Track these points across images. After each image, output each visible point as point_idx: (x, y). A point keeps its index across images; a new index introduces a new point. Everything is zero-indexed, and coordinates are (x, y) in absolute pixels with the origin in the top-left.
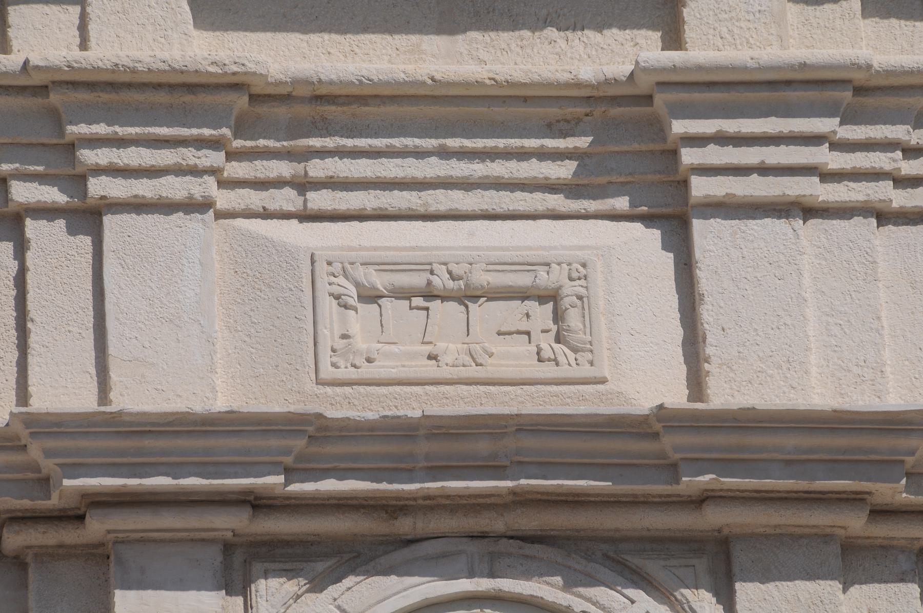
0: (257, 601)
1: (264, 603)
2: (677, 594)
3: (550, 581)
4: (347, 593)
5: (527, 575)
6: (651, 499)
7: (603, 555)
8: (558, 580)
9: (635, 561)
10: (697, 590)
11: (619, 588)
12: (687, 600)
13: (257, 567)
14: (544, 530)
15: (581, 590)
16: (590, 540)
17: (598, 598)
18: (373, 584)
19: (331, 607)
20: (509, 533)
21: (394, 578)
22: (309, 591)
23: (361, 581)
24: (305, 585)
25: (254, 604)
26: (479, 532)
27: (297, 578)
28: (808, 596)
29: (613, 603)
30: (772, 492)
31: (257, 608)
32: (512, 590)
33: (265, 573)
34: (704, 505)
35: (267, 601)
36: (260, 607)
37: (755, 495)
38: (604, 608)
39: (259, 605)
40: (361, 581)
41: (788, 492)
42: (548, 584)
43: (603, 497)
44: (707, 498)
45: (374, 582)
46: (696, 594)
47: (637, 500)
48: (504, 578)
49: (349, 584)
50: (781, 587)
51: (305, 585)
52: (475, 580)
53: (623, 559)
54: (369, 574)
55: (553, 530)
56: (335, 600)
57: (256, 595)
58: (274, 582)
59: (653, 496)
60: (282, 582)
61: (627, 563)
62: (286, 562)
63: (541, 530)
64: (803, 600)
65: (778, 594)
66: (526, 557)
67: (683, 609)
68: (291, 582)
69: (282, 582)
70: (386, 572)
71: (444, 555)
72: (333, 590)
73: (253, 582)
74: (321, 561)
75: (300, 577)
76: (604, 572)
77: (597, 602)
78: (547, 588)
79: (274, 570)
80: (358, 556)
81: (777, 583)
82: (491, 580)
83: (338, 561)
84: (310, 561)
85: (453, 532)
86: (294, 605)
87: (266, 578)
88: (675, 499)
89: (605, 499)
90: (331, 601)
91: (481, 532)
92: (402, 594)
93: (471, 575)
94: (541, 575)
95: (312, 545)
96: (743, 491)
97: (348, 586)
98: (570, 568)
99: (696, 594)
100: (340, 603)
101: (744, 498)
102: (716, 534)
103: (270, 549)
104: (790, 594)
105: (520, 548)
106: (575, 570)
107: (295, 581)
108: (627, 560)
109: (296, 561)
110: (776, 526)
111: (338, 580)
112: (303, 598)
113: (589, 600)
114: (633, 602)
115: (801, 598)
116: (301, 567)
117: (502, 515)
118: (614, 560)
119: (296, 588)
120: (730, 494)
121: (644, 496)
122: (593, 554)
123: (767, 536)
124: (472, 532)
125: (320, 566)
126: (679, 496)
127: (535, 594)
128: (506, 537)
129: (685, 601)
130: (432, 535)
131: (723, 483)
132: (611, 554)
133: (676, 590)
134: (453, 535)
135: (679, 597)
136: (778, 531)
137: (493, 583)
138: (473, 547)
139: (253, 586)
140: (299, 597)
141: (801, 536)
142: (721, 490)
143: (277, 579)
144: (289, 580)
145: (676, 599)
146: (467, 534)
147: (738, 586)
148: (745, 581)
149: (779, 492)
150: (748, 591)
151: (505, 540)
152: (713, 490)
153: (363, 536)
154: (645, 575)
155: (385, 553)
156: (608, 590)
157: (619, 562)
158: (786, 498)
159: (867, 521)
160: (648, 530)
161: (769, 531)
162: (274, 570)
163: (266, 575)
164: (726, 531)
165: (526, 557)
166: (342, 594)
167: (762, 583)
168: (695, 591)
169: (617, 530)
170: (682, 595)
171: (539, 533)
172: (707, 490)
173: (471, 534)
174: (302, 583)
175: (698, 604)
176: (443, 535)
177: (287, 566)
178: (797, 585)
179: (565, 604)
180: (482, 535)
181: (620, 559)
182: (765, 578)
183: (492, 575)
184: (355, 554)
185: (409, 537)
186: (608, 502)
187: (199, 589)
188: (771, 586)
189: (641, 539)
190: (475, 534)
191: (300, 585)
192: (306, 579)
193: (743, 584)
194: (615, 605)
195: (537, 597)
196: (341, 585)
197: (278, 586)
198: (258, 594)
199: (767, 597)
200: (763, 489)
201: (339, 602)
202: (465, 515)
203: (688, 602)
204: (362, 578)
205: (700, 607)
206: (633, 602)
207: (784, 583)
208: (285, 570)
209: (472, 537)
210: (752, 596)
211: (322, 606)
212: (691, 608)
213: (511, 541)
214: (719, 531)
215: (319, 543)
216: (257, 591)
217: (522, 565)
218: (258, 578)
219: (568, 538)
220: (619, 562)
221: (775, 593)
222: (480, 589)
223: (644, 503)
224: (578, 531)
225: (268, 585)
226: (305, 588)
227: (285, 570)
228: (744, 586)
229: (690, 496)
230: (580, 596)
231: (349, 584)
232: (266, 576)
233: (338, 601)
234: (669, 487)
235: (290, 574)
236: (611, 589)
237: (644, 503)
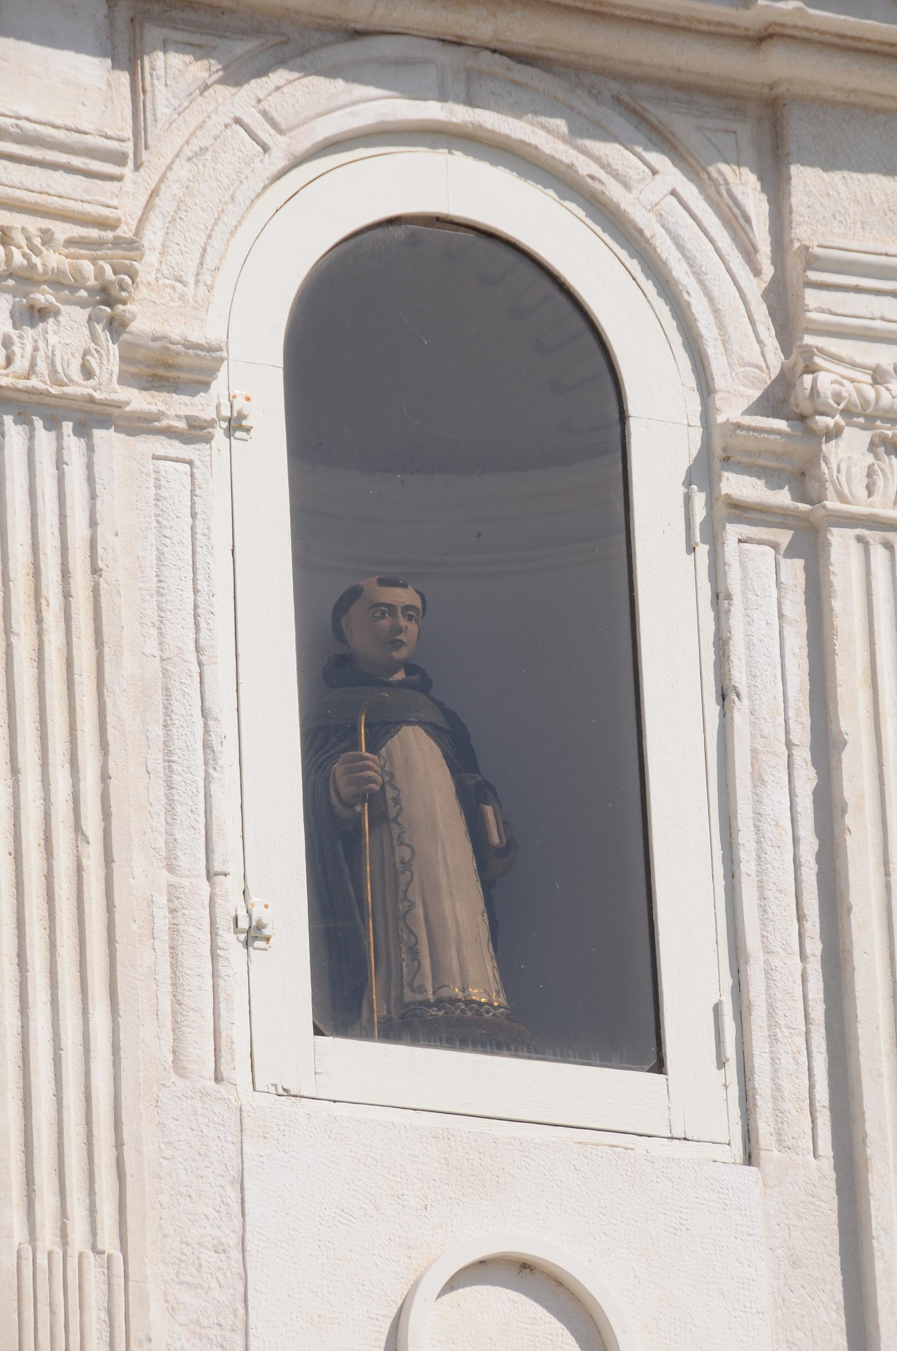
0: (152, 84)
1: (162, 88)
2: (711, 169)
3: (547, 125)
4: (275, 94)
5: (516, 110)
6: (695, 25)
7: (613, 97)
8: (561, 124)
9: (658, 113)
10: (739, 167)
11: (639, 149)
12: (725, 180)
13: (153, 32)
14: (541, 48)
15: (589, 143)
16: (596, 73)
17: (610, 160)
18: (311, 88)
19: (254, 110)
20: (493, 45)
21: (340, 83)
22: (221, 81)
23: (294, 81)
24: (217, 71)
25: (148, 87)
26: (453, 36)
27: (207, 58)
28: (883, 198)
29: (630, 170)
30: (860, 39)
31: (153, 94)
32: (497, 129)
33: (164, 44)
34: (765, 45)
35: (166, 85)
36: (157, 93)
37: (837, 40)
38: (617, 174)
39: (156, 89)
40: (294, 81)
41: (880, 43)
42: (543, 127)
43: (634, 11)
44: (771, 36)
45: (312, 85)
46: (738, 172)
47: (677, 23)
48: (485, 108)
49: (279, 82)
50: (849, 181)
51: (217, 71)
52: (450, 105)
53: (644, 108)
54: (307, 71)
55: (551, 49)
56: (259, 101)
57: (151, 75)
58: (177, 60)
59: (700, 22)
60: (188, 62)
61: (647, 115)
62: (192, 32)
63: (537, 47)
64: (877, 203)
65: (845, 189)
66: (515, 83)
67: (719, 193)
68: (199, 63)
69: (188, 62)
70: (331, 72)
71: (405, 62)
72: (257, 87)
73: (149, 53)
74: (240, 39)
75: (213, 58)
76: (618, 122)
77: (609, 165)
78: (542, 133)
79: (176, 42)
80: (285, 43)
81: (845, 173)
82: (469, 109)
83: (262, 45)
84: (226, 37)
85: (419, 30)
86: (200, 100)
87: (165, 51)
88: (726, 30)
89: (634, 15)
90: (254, 102)
91: (457, 37)
92: (349, 110)
93: (443, 97)
94: (536, 113)
95: (223, 13)
96: (823, 33)
97: (278, 84)
98: (572, 108)
99: (738, 172)
100: (267, 108)
101: (821, 43)
102: (766, 90)
103: (165, 8)
104: (861, 191)
105: (508, 69)
106: (580, 113)
107: (205, 62)
108: (646, 110)
109: (206, 34)
110: (851, 91)
111: (262, 72)
112: (211, 90)
113: (597, 160)
114: (654, 172)
115: (875, 200)
116: (214, 45)
117: (494, 15)
118: (627, 107)
119: (205, 74)
120: (806, 34)
121: (687, 18)
122: (599, 93)
123: (834, 104)
124: (444, 34)
125: (240, 47)
126: (733, 26)
127: (527, 140)
128: (487, 48)
129: (722, 182)
130: (389, 29)
131: (810, 16)
132: (626, 98)
133: (710, 164)
134: (419, 33)
135: (715, 175)
136: (852, 99)
137: (472, 114)
138: (446, 56)
139: (146, 59)
140: (207, 87)
141: (878, 111)
142: (795, 27)
143: (181, 56)
144: (197, 59)
145: (710, 177)
146: (437, 36)
147: (795, 170)
148: (803, 165)
149: (869, 41)
150: (807, 180)
151: (487, 54)
152: (783, 25)
153: (297, 12)
154: (669, 136)
155: (323, 45)
156: (621, 148)
157: (634, 112)
158: (875, 52)
159: (132, 320)
160: (679, 70)
161: (841, 97)
162: (176, 42)
163: (165, 47)
164: (781, 89)
165: (515, 83)
166: (269, 95)
167: (825, 170)
168: (736, 168)
169: (639, 64)
170: (720, 172)
171: (534, 51)
172: (776, 24)
173: (443, 37)
174: (214, 69)
175: (740, 188)
176: (406, 31)
177: (195, 39)
178: (871, 181)
179: (567, 161)
180: (458, 40)
181: (638, 108)
182: (829, 165)
183: (470, 102)
184: (283, 39)
185: (359, 27)
186: (638, 20)
187: (78, 50)
188: (836, 176)
189: (662, 82)
190: (448, 38)
191: (212, 70)
192: (220, 62)
193: (802, 168)
194: (632, 173)
195: (530, 145)
196: (268, 81)
197: (181, 66)
198: (154, 73)
199: (831, 193)
200: (850, 33)
201: (265, 105)
202: (444, 7)
203: (727, 183)
204: (296, 75)
205: (743, 193)
206: (654, 172)
207: (854, 175)
208: (190, 44)
209: (443, 41)
210: (812, 188)
211: (242, 108)
212: (730, 193)
213: (496, 56)
214: (771, 87)
215: (233, 12)
216: (152, 69)
217: (510, 94)
218: (155, 49)
219: (567, 65)
220: (634, 112)
221: (842, 188)
222: (454, 120)
223: (685, 29)
224: (586, 56)
225: (169, 62)
226: (216, 77)
227: (190, 44)
228: (801, 171)
229: (747, 29)
230: (585, 152)
231: (279, 82)
232: (165, 47)
233: (263, 103)
234: (733, 11)
235: (199, 51)
236: (626, 148)
237: (685, 29)
